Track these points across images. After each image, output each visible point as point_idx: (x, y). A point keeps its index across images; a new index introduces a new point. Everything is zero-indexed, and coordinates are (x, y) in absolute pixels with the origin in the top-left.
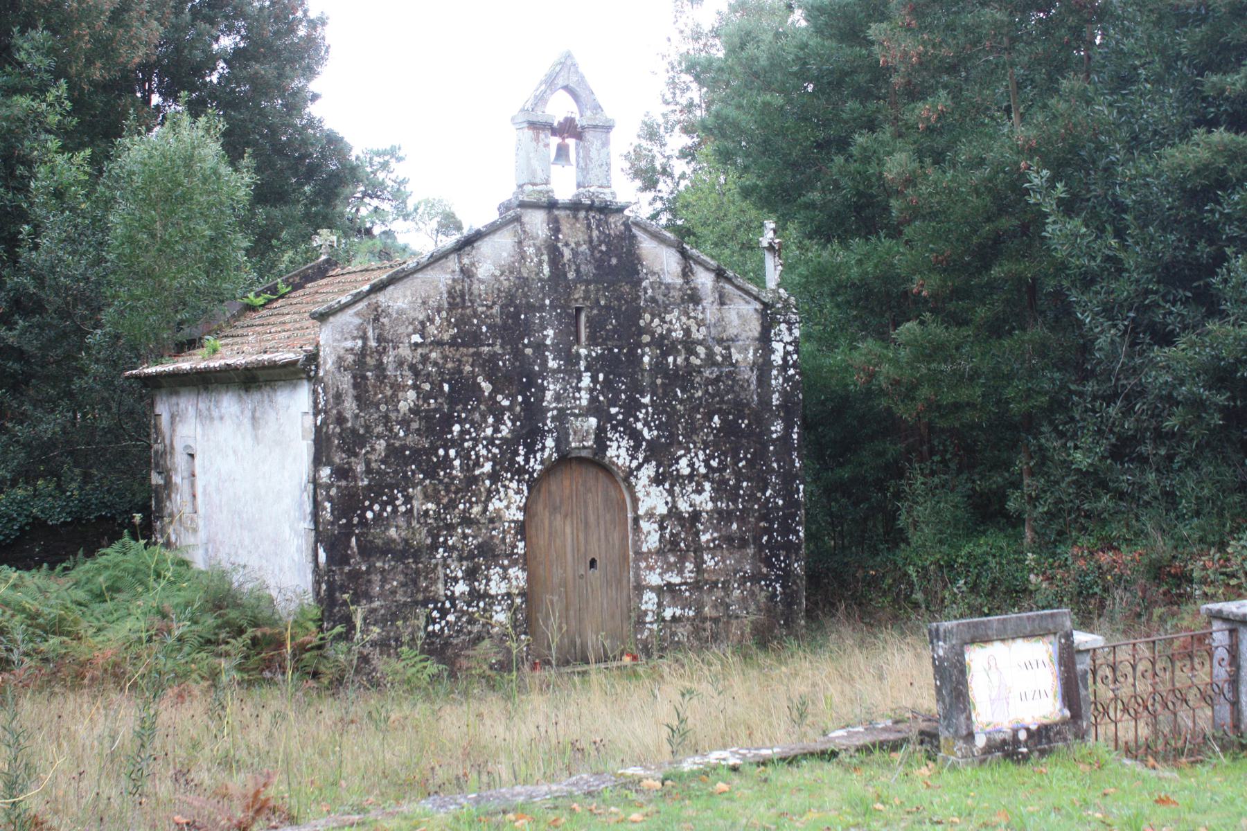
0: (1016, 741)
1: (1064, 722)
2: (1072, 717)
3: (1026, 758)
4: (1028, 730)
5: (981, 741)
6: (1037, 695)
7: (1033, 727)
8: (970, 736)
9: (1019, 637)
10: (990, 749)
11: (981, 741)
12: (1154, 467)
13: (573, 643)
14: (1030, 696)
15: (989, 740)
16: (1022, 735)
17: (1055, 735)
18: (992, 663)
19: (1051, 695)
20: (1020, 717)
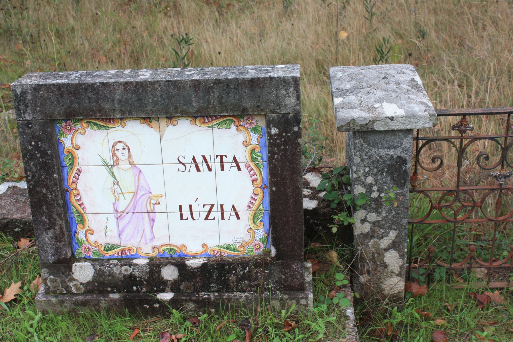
0: (153, 279)
1: (262, 262)
2: (278, 256)
3: (164, 310)
4: (180, 264)
5: (83, 272)
6: (216, 213)
7: (194, 263)
8: (63, 265)
9: (185, 114)
10: (100, 285)
11: (83, 272)
12: (488, 325)
13: (489, 121)
14: (200, 213)
15: (99, 274)
16: (169, 273)
17: (239, 280)
18: (122, 155)
19: (246, 216)
20: (177, 241)
